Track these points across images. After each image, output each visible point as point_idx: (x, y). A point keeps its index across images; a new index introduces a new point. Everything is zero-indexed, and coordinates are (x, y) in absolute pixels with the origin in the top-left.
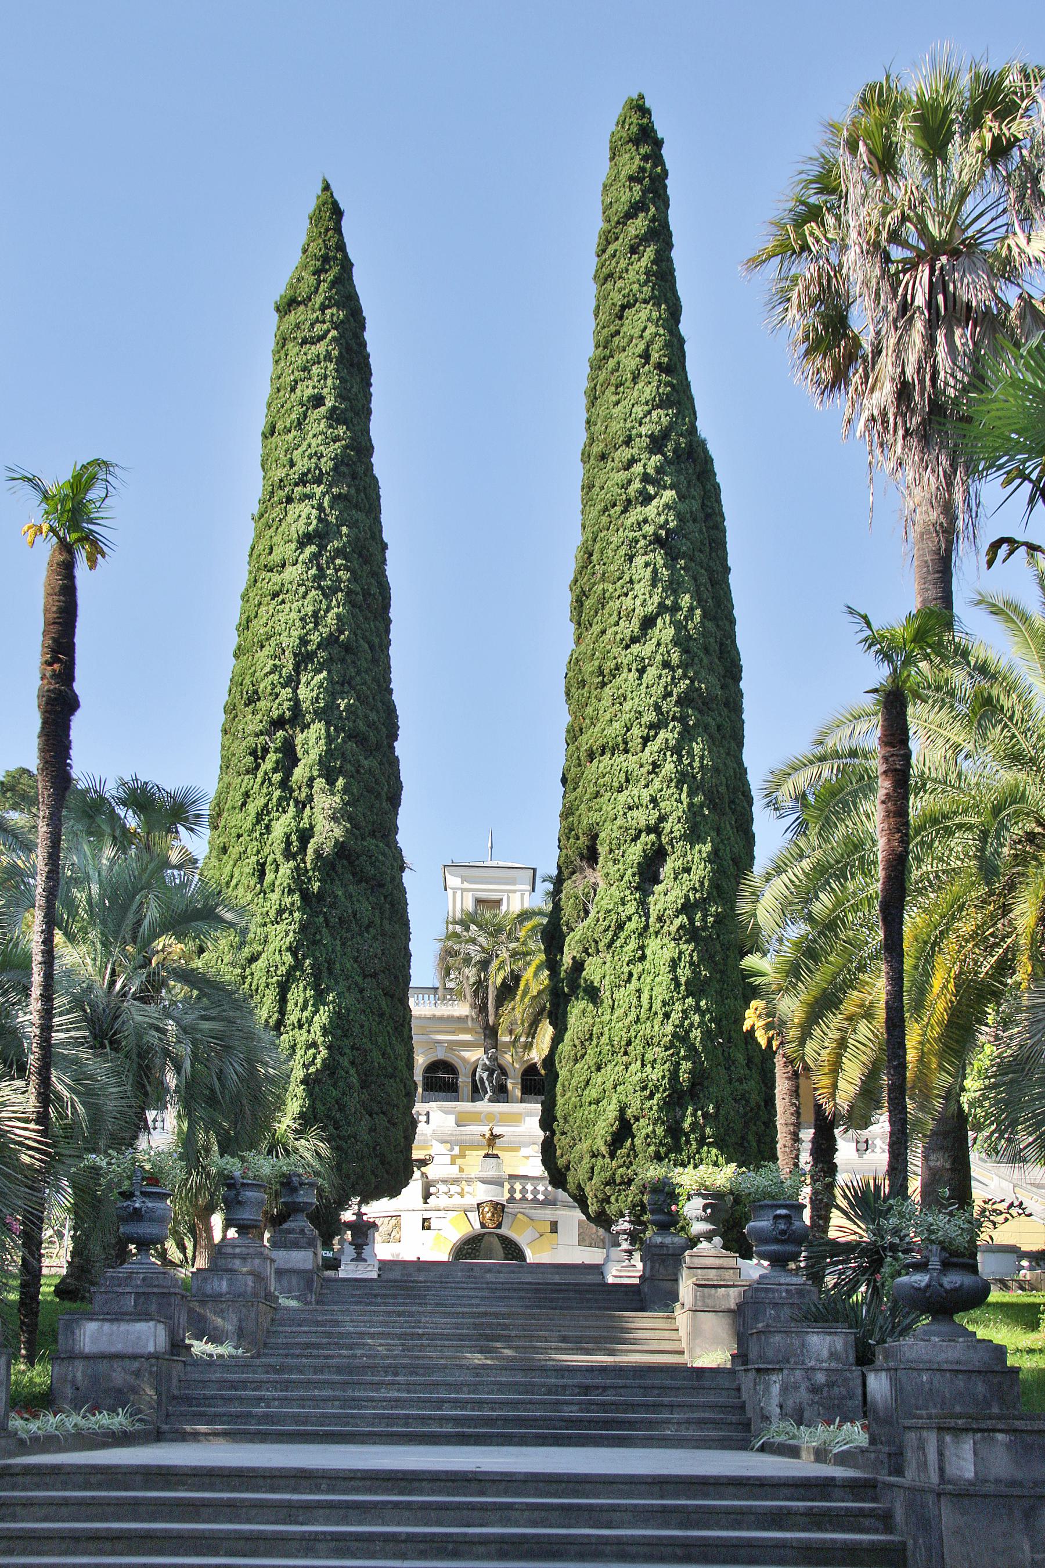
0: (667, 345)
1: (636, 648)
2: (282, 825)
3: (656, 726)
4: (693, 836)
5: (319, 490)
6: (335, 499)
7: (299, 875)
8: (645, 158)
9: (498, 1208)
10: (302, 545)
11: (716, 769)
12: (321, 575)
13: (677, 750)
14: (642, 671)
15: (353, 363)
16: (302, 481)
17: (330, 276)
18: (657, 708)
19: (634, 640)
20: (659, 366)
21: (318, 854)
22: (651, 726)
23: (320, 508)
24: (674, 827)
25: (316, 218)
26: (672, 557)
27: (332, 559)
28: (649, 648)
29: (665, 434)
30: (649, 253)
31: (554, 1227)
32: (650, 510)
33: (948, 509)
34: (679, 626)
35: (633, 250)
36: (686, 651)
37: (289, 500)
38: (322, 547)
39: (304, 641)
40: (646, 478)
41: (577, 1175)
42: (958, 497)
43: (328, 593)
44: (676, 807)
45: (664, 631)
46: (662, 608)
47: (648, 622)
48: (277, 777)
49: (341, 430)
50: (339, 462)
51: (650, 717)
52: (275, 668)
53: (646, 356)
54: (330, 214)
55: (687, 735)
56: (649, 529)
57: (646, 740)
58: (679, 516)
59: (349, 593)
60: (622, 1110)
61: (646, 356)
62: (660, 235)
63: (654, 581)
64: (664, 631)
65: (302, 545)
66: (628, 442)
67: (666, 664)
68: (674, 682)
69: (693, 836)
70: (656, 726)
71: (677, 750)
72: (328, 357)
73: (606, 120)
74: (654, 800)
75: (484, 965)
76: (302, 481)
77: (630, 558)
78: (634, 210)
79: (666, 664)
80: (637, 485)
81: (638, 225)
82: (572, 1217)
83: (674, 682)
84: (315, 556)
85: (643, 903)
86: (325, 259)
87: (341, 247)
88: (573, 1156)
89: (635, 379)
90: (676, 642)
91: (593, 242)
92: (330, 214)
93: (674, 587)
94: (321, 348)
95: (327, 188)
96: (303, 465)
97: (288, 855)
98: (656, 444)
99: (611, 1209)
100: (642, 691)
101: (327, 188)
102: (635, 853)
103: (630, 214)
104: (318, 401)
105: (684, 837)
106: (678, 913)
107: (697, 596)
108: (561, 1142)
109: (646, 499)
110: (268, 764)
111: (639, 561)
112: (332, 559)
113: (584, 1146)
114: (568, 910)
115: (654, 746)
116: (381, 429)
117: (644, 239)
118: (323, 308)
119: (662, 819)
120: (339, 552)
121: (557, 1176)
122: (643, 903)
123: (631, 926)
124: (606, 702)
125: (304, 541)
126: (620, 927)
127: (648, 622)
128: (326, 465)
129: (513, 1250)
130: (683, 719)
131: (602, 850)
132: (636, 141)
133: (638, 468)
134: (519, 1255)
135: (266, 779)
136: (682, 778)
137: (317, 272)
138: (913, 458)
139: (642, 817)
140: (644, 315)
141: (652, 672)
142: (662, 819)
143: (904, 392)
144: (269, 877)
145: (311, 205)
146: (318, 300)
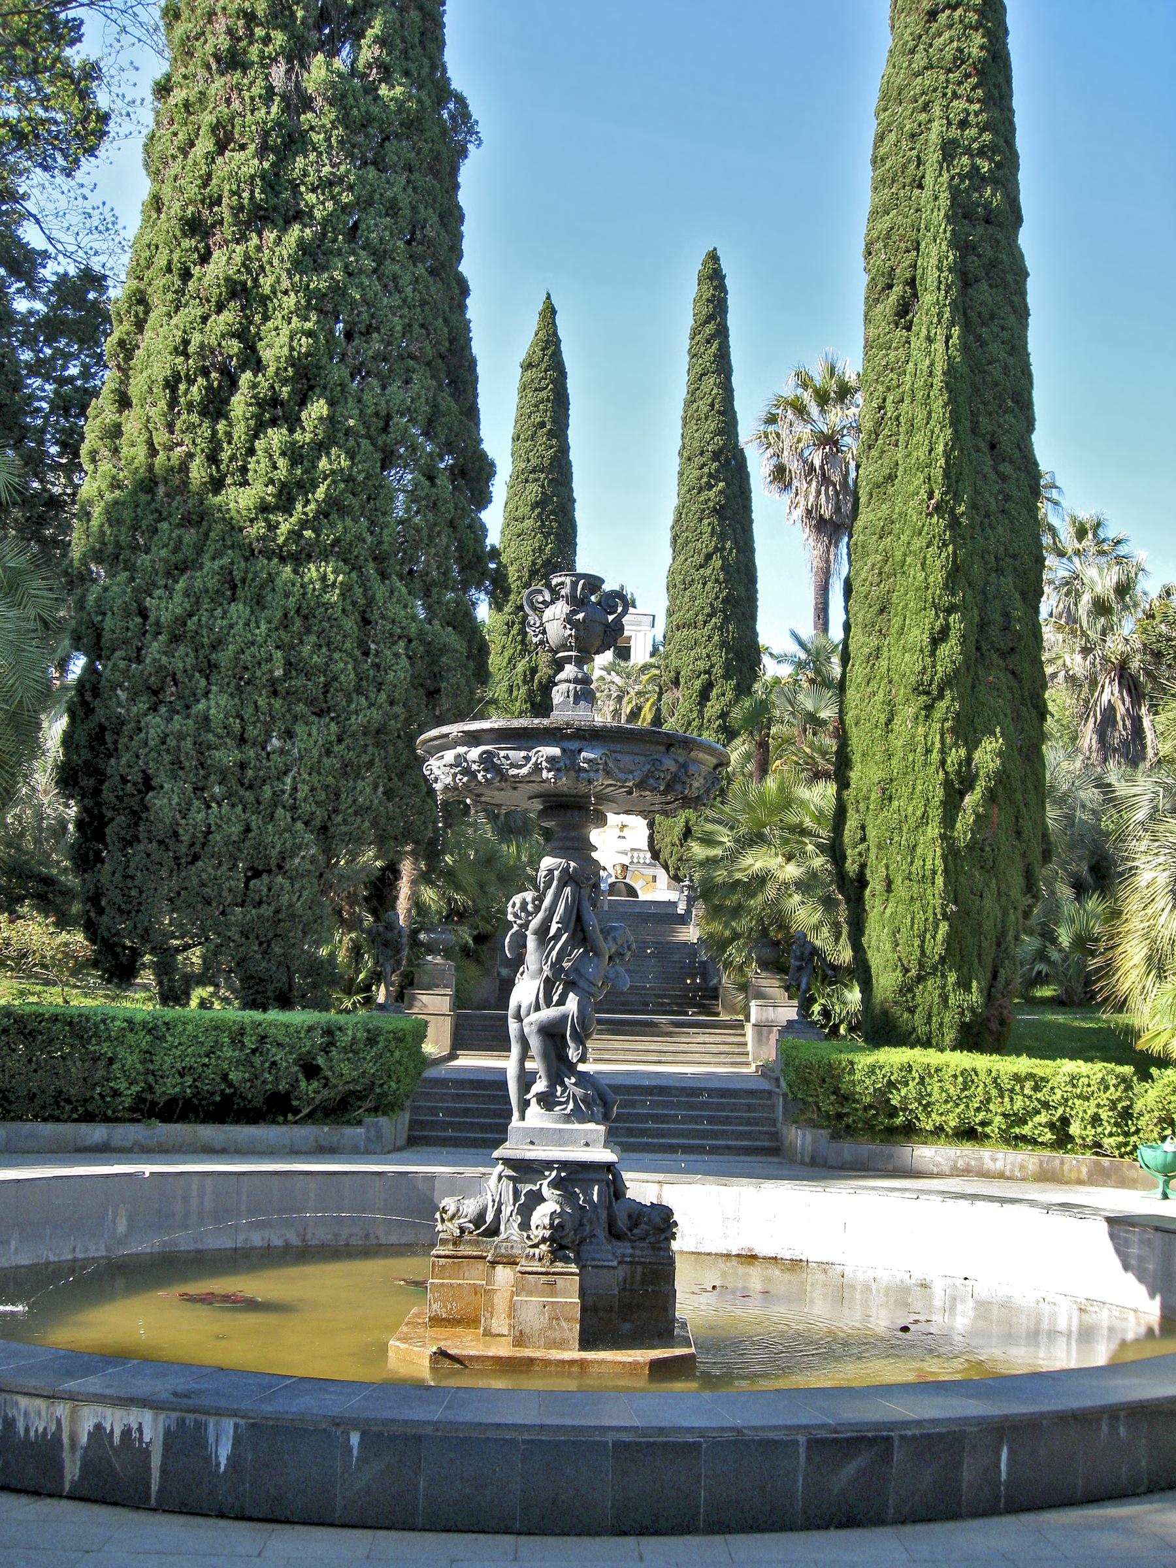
0: (723, 400)
1: (702, 571)
2: (521, 666)
3: (710, 616)
4: (727, 676)
5: (543, 476)
6: (551, 481)
7: (530, 692)
8: (715, 289)
9: (625, 868)
10: (533, 510)
11: (740, 638)
12: (543, 526)
13: (721, 629)
14: (705, 584)
15: (560, 401)
16: (534, 471)
17: (549, 352)
18: (711, 605)
19: (702, 566)
20: (719, 412)
21: (540, 683)
22: (708, 615)
23: (543, 486)
24: (718, 671)
25: (543, 315)
26: (722, 518)
27: (548, 517)
28: (708, 572)
29: (721, 450)
30: (715, 345)
31: (654, 877)
32: (712, 494)
33: (828, 561)
34: (723, 558)
35: (708, 342)
36: (727, 573)
37: (527, 481)
38: (543, 509)
39: (534, 563)
40: (710, 475)
41: (665, 854)
42: (832, 557)
43: (546, 536)
44: (719, 659)
45: (717, 562)
46: (716, 549)
47: (709, 557)
48: (519, 638)
49: (554, 442)
50: (553, 459)
51: (708, 610)
52: (519, 578)
53: (712, 405)
54: (549, 312)
55: (726, 620)
56: (711, 504)
57: (705, 622)
58: (727, 498)
59: (557, 535)
60: (687, 822)
61: (712, 405)
62: (722, 333)
63: (712, 534)
64: (717, 562)
65: (533, 510)
66: (702, 454)
67: (717, 581)
68: (721, 591)
69: (727, 676)
70: (710, 616)
71: (721, 629)
72: (548, 400)
73: (695, 265)
74: (708, 656)
75: (619, 699)
76: (534, 471)
77: (701, 520)
78: (710, 318)
79: (717, 581)
80: (705, 479)
81: (710, 329)
82: (661, 874)
83: (721, 591)
84: (540, 514)
85: (701, 712)
86: (547, 342)
87: (555, 334)
88: (662, 845)
89: (706, 418)
90: (722, 569)
91: (687, 332)
92: (549, 312)
93: (722, 537)
94: (544, 394)
95: (548, 297)
96: (534, 462)
97: (525, 682)
98: (716, 456)
99: (680, 874)
100: (706, 595)
101: (548, 297)
102: (698, 684)
103: (707, 322)
104: (542, 425)
105: (723, 677)
106: (719, 717)
107: (735, 542)
108: (657, 837)
109: (710, 487)
110: (514, 632)
111: (706, 522)
112: (548, 517)
113: (668, 840)
114: (664, 712)
115: (710, 626)
116: (575, 435)
117: (713, 336)
118: (546, 371)
119: (712, 666)
120: (552, 512)
121: (655, 855)
122: (701, 712)
123: (694, 724)
124: (686, 599)
125: (536, 505)
126: (689, 724)
127: (709, 557)
128: (546, 462)
129: (632, 892)
130: (724, 611)
131: (682, 681)
132: (711, 278)
133: (706, 470)
134: (635, 895)
135: (514, 639)
136: (723, 644)
137: (543, 350)
138: (813, 536)
139: (702, 665)
140: (712, 381)
141: (710, 584)
142: (712, 666)
143: (809, 512)
144: (515, 693)
145: (540, 307)
146: (544, 366)
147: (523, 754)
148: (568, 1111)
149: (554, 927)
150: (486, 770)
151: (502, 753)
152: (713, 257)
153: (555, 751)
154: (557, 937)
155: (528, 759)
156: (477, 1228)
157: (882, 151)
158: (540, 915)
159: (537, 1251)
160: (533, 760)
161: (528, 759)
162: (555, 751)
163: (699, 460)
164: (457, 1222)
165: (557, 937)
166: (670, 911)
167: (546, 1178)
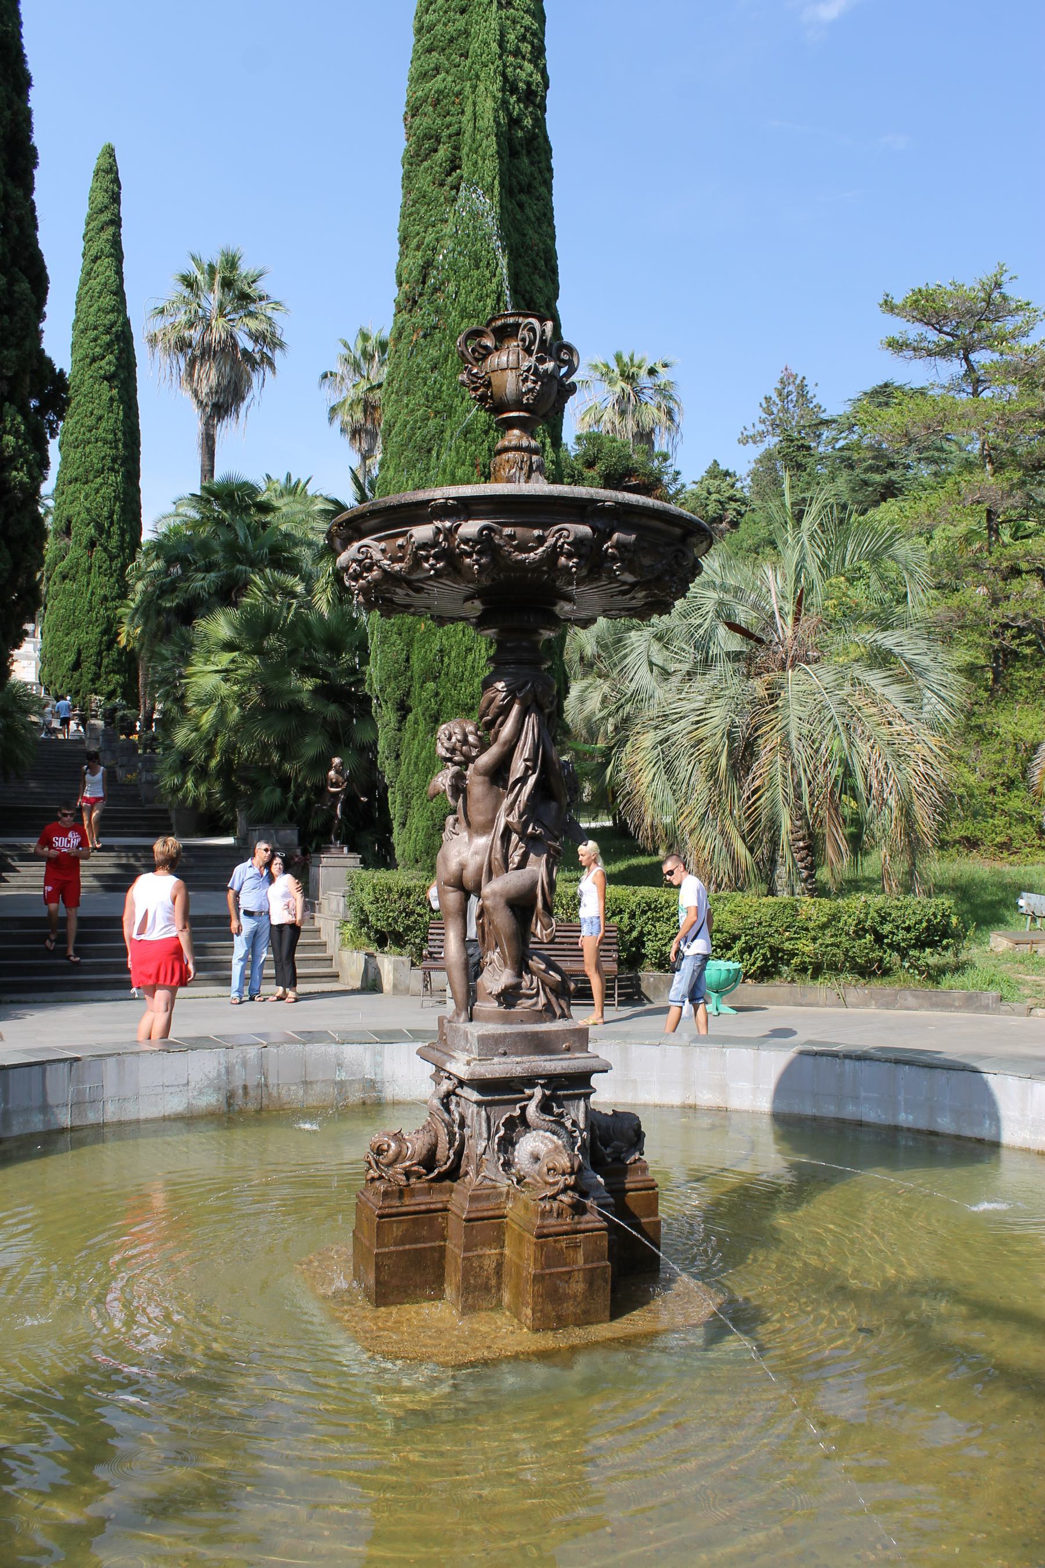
81: (105, 217)
103: (101, 211)
147: (537, 532)
148: (539, 1007)
149: (518, 767)
150: (480, 553)
151: (507, 531)
152: (110, 152)
153: (585, 530)
154: (523, 780)
155: (541, 540)
156: (430, 1170)
157: (428, 18)
158: (494, 751)
159: (555, 1205)
160: (551, 541)
161: (541, 540)
162: (585, 530)
163: (92, 334)
164: (399, 1167)
165: (523, 780)
166: (80, 747)
167: (530, 1098)
